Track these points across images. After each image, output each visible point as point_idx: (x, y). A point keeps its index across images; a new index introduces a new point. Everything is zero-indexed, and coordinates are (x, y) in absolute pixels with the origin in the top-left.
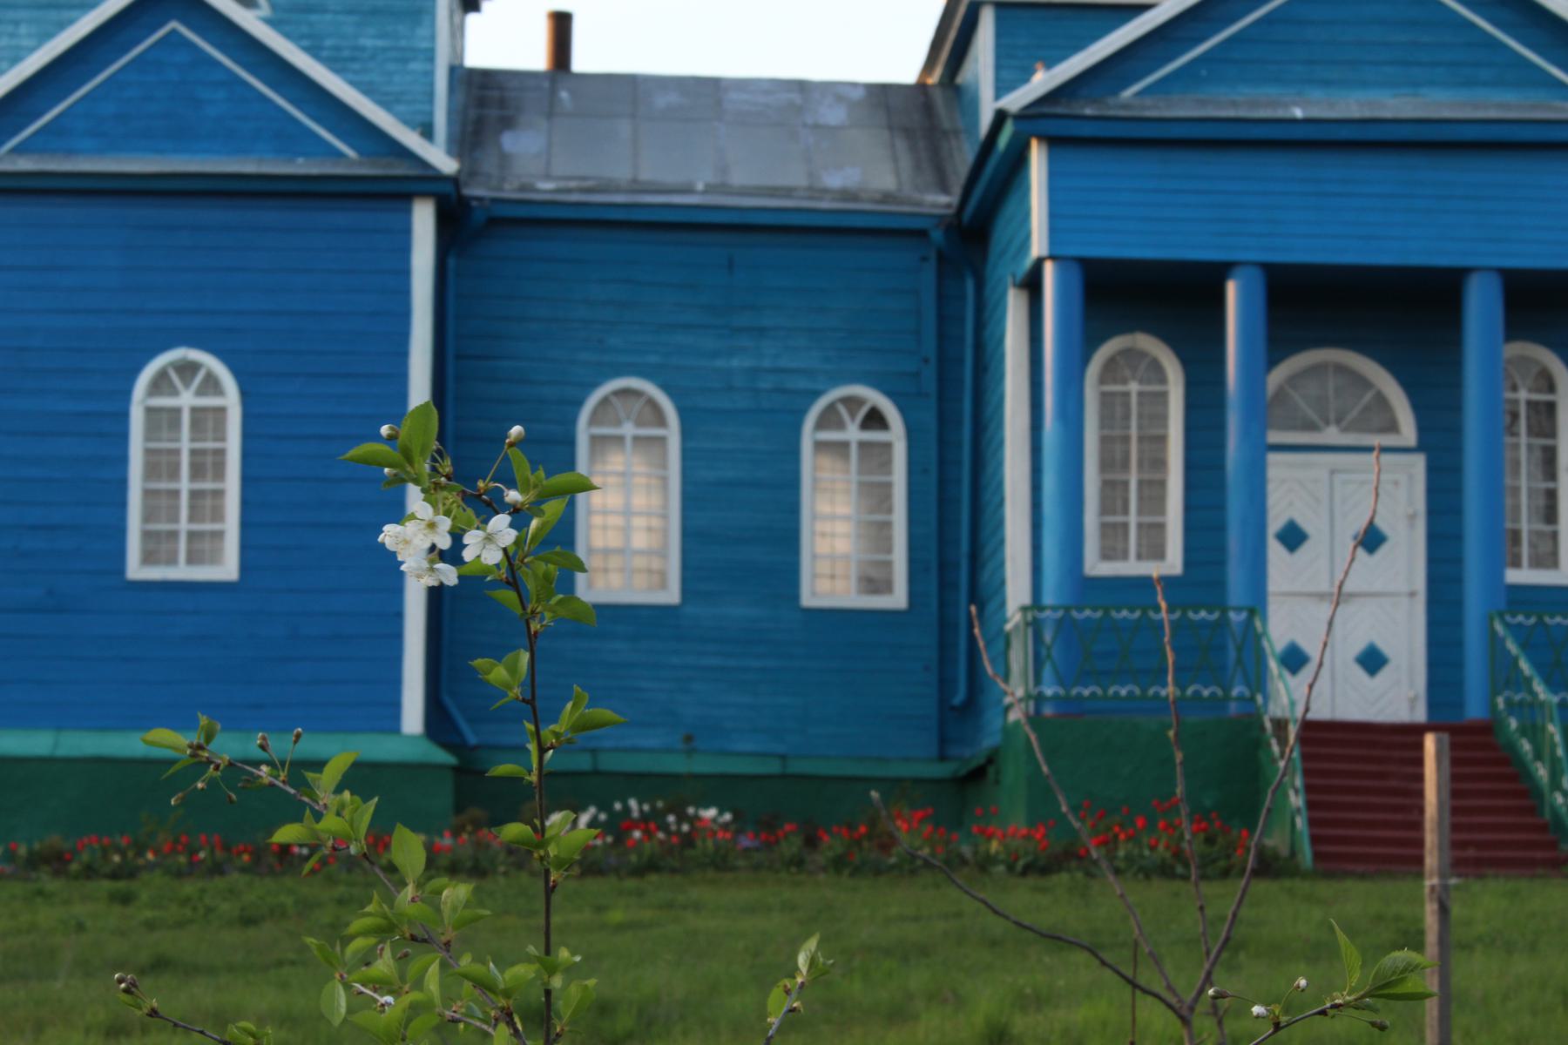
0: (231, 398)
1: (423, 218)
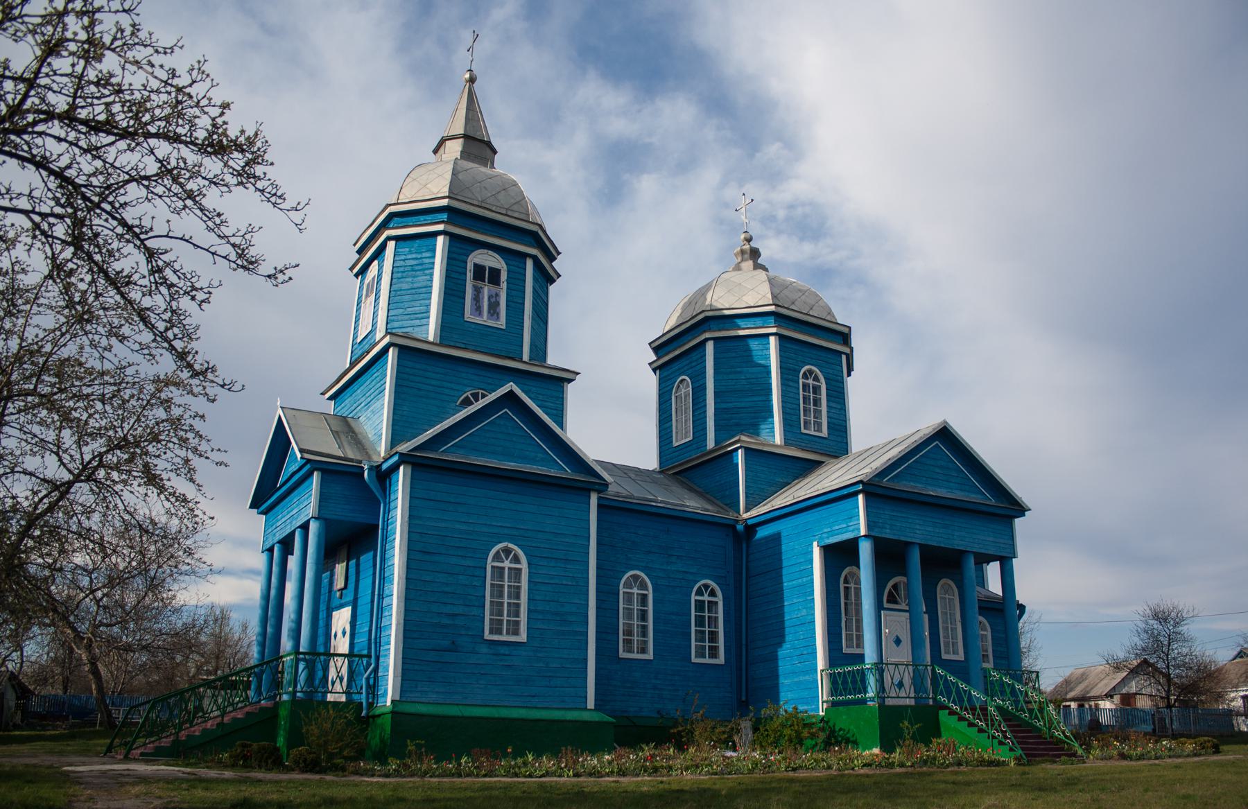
0: (524, 565)
1: (861, 497)
